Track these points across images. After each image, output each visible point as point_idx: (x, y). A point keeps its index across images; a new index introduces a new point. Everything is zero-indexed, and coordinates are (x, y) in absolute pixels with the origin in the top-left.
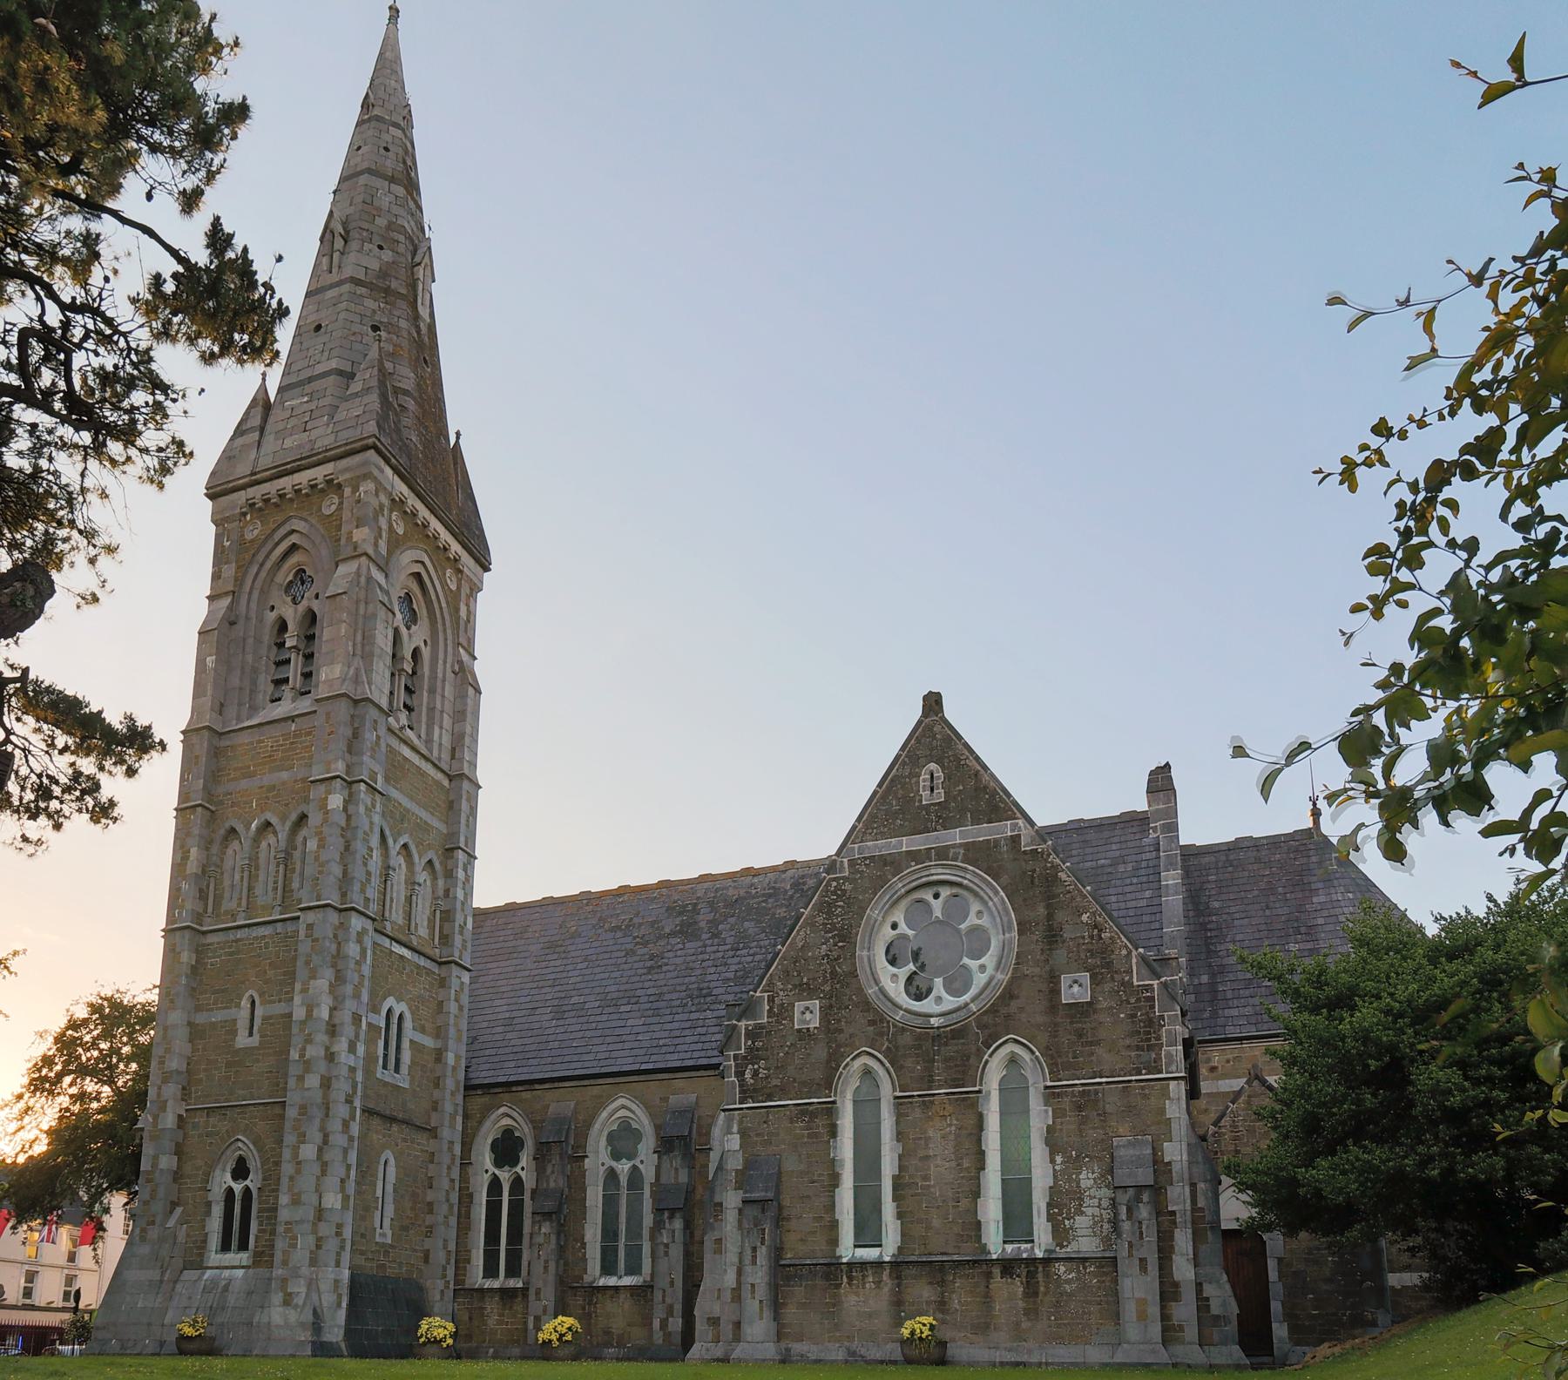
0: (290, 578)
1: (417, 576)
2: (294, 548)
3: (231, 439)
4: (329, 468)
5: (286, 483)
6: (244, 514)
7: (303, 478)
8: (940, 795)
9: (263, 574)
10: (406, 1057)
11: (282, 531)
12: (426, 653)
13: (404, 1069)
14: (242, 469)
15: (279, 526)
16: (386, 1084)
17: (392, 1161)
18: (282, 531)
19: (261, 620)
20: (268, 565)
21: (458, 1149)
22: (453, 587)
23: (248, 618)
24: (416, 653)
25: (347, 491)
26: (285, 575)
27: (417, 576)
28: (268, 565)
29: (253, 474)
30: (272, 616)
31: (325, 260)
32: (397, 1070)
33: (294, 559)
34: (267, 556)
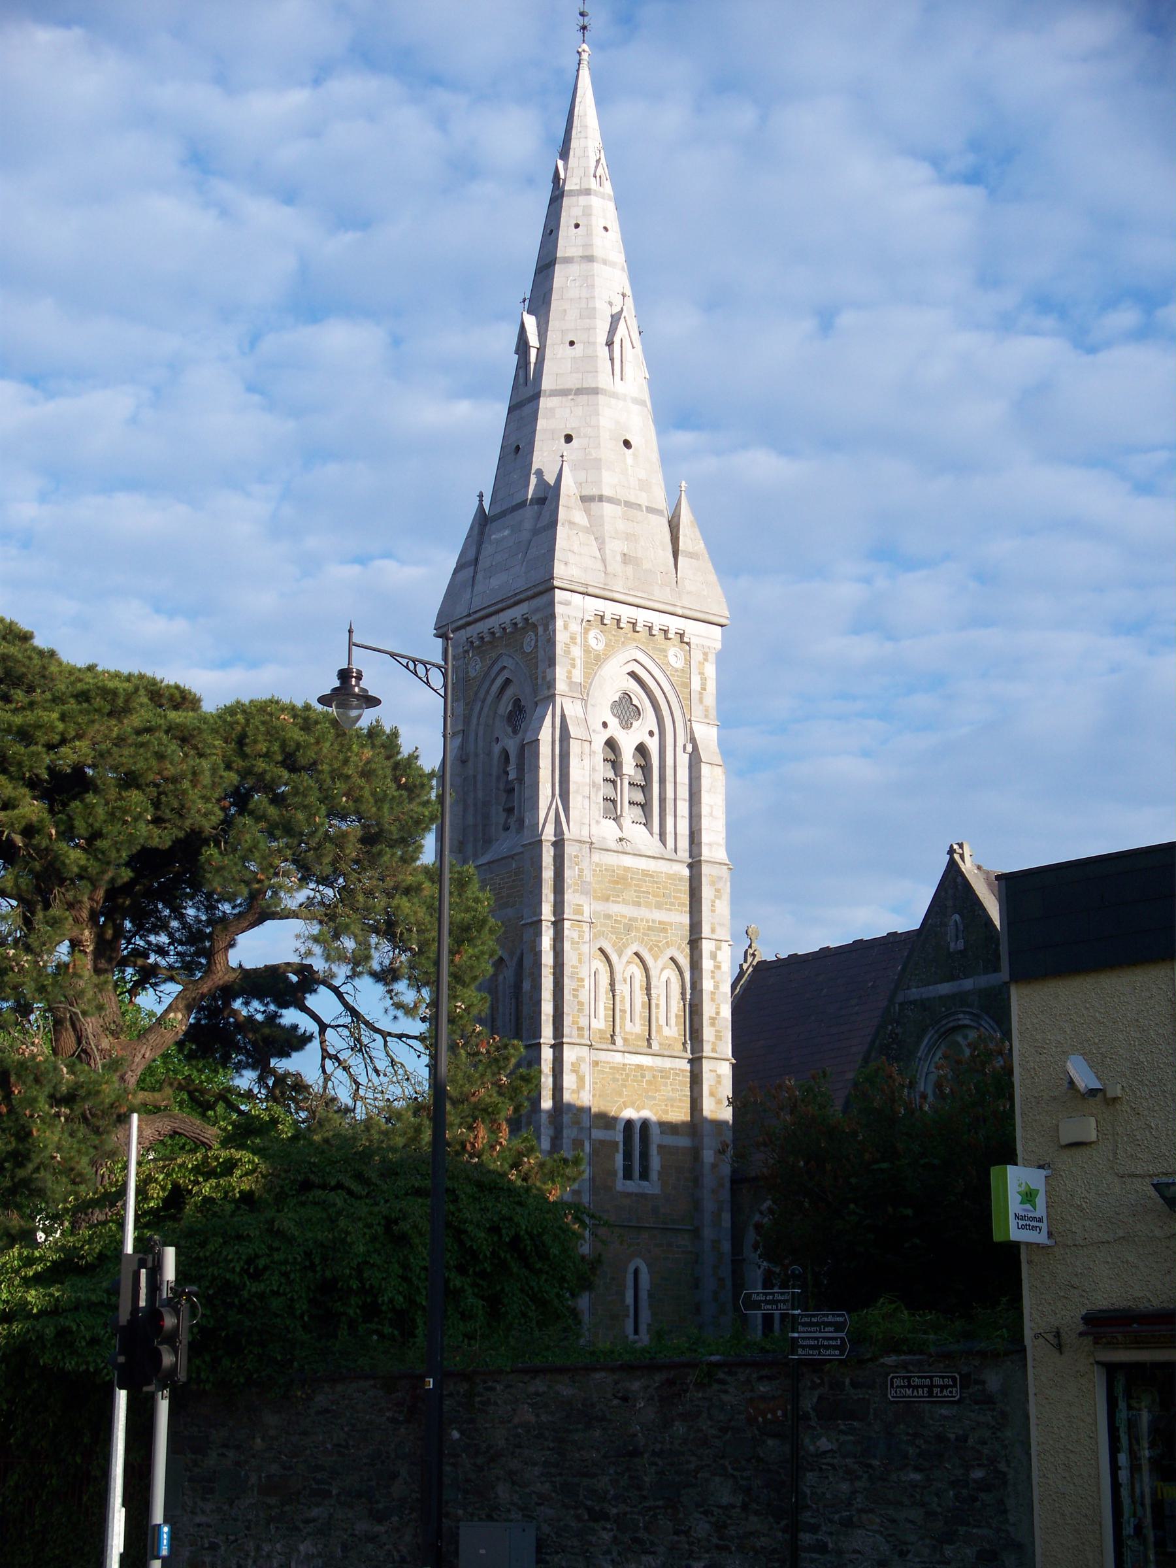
0: (510, 708)
1: (633, 675)
2: (508, 682)
3: (456, 571)
4: (523, 609)
5: (493, 622)
6: (467, 652)
7: (506, 617)
8: (961, 945)
9: (486, 710)
10: (655, 1162)
11: (496, 668)
12: (653, 745)
13: (654, 1175)
14: (461, 610)
15: (493, 664)
16: (629, 1195)
17: (644, 1269)
18: (496, 668)
19: (489, 754)
20: (489, 699)
21: (726, 1246)
22: (678, 664)
23: (476, 755)
24: (641, 750)
25: (540, 629)
26: (505, 706)
27: (633, 675)
28: (489, 699)
29: (469, 615)
30: (497, 749)
31: (521, 373)
32: (644, 1175)
33: (510, 692)
34: (487, 692)
